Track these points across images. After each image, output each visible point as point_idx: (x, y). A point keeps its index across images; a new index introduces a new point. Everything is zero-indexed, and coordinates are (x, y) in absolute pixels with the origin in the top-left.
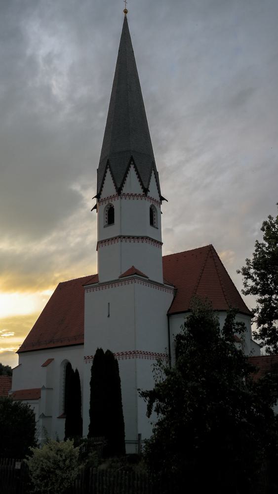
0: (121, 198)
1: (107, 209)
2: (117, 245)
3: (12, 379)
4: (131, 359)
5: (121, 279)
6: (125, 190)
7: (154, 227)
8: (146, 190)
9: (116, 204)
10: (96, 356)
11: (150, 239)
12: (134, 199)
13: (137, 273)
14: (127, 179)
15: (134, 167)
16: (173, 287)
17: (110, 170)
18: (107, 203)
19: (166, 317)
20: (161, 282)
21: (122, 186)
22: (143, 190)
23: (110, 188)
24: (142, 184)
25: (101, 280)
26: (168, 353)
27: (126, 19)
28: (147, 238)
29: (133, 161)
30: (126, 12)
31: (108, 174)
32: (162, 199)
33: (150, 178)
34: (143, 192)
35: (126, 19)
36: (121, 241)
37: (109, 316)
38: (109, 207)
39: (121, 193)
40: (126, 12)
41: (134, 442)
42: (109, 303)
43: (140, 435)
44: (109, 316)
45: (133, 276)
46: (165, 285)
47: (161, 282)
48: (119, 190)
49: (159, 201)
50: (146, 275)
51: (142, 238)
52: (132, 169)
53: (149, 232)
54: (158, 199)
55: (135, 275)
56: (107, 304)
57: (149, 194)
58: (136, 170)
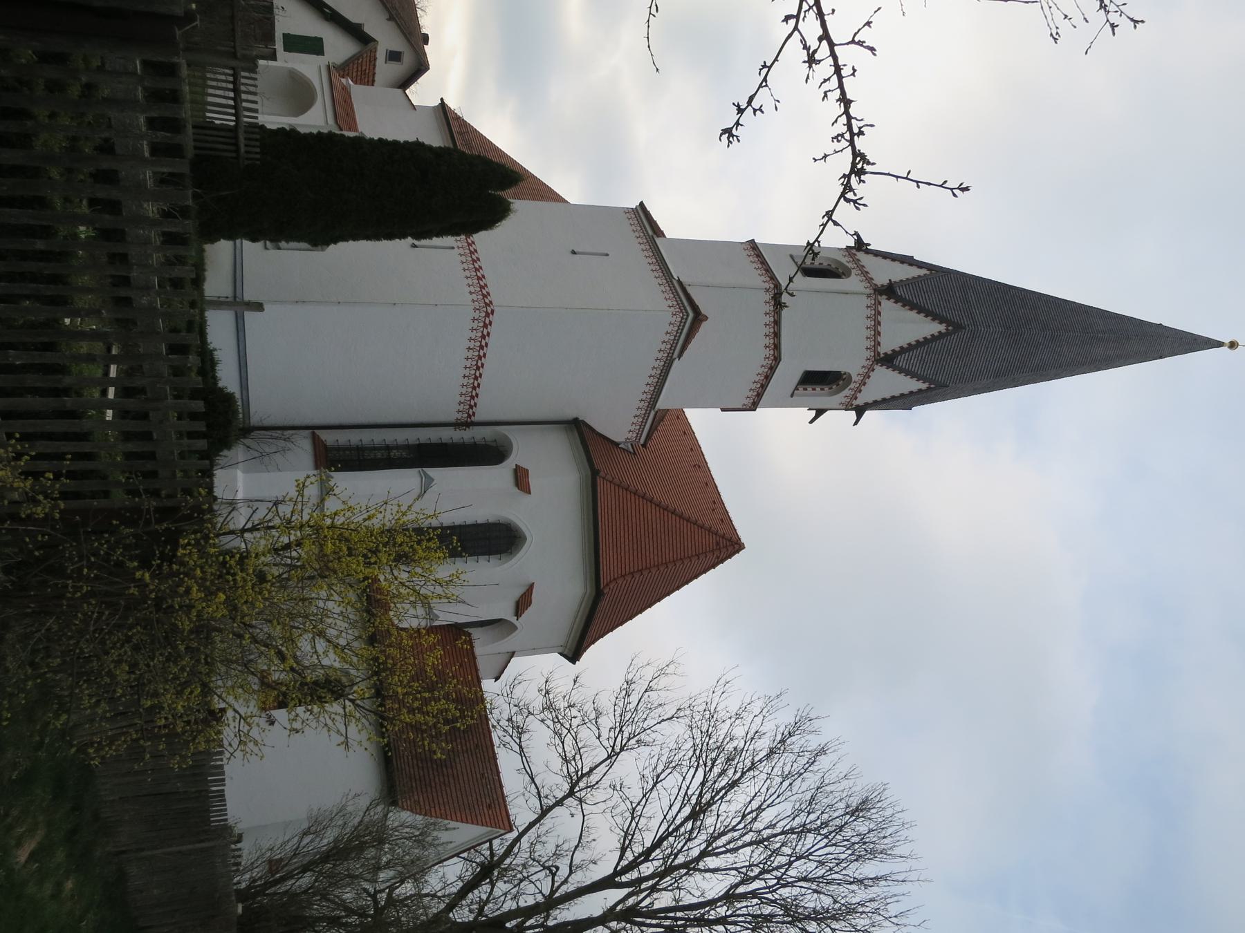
0: (869, 296)
1: (833, 266)
2: (757, 279)
3: (368, 85)
4: (470, 297)
5: (675, 282)
6: (888, 307)
7: (796, 389)
8: (888, 360)
9: (853, 283)
10: (454, 231)
11: (772, 369)
12: (867, 328)
13: (699, 318)
14: (913, 314)
15: (940, 332)
16: (642, 441)
17: (920, 390)
18: (850, 265)
19: (570, 414)
20: (661, 405)
21: (898, 299)
22: (889, 352)
23: (884, 274)
24: (903, 350)
25: (659, 241)
26: (476, 419)
27: (1219, 344)
28: (777, 359)
29: (954, 332)
30: (1233, 345)
31: (923, 272)
32: (860, 412)
33: (913, 375)
34: (885, 354)
35: (1219, 344)
36: (767, 290)
37: (574, 252)
38: (840, 271)
39: (881, 295)
40: (1233, 345)
41: (239, 294)
42: (607, 255)
43: (259, 307)
44: (574, 252)
45: (689, 309)
46: (653, 413)
47: (661, 405)
48: (889, 291)
49: (855, 403)
50: (686, 353)
51: (777, 347)
52: (935, 328)
53: (788, 373)
54: (860, 401)
55: (691, 315)
56: (606, 252)
57: (878, 368)
58: (934, 338)
